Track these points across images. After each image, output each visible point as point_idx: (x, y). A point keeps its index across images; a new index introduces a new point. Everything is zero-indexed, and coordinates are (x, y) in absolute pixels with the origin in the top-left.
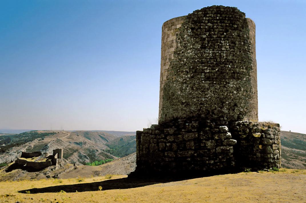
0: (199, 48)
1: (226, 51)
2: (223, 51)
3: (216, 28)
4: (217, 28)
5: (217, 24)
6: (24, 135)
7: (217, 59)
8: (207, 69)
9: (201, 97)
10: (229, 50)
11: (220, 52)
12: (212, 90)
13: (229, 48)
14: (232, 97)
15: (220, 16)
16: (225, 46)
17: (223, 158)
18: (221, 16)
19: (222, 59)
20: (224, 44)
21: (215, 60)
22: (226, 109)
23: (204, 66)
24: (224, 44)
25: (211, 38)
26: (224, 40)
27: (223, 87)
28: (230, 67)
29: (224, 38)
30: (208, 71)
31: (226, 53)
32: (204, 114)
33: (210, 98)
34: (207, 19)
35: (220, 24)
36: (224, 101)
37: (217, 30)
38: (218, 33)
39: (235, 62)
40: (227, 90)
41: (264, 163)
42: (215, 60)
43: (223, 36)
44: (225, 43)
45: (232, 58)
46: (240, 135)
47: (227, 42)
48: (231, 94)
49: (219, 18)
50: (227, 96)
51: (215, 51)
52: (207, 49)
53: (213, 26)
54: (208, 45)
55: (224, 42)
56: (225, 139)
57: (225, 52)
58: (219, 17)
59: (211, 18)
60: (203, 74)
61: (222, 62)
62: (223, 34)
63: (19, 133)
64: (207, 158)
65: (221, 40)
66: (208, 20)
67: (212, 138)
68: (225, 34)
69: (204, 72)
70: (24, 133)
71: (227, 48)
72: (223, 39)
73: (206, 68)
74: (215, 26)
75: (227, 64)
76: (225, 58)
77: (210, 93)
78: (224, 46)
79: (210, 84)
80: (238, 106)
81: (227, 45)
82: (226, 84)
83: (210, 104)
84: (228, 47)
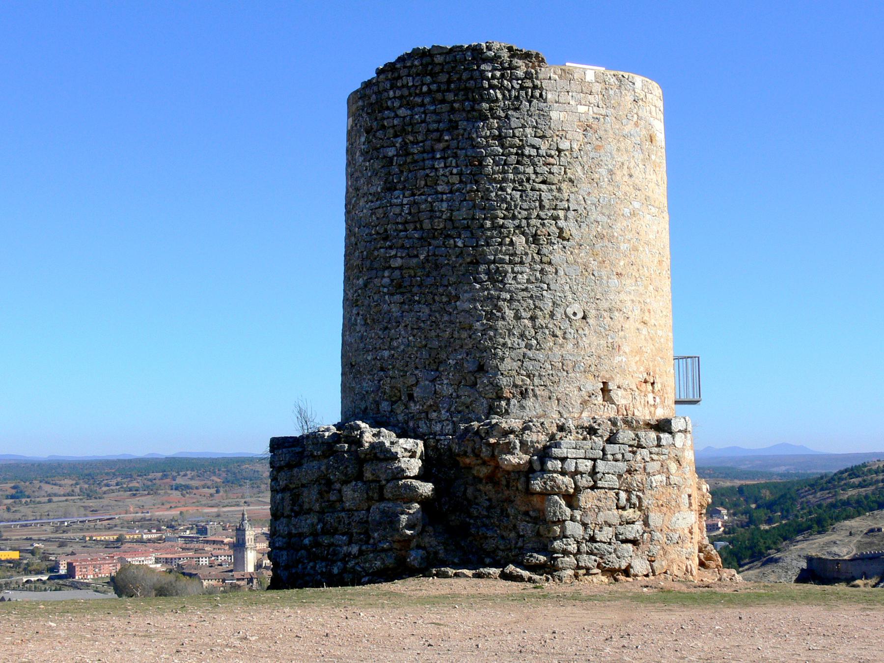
0: (379, 190)
1: (451, 192)
2: (440, 196)
3: (418, 123)
4: (423, 122)
5: (422, 109)
6: (856, 481)
7: (421, 222)
8: (395, 256)
9: (382, 347)
10: (458, 190)
11: (429, 199)
12: (408, 322)
13: (461, 182)
14: (466, 344)
15: (434, 82)
16: (447, 177)
17: (384, 539)
18: (434, 79)
19: (436, 220)
20: (441, 172)
21: (418, 226)
22: (445, 382)
23: (391, 248)
24: (441, 172)
25: (408, 154)
26: (444, 158)
27: (439, 312)
28: (460, 244)
29: (444, 150)
30: (398, 262)
31: (448, 201)
32: (386, 400)
33: (402, 347)
34: (398, 93)
35: (432, 108)
36: (443, 356)
37: (423, 128)
38: (426, 135)
39: (482, 226)
40: (451, 322)
41: (545, 562)
42: (418, 226)
43: (441, 145)
44: (446, 167)
45: (468, 214)
46: (469, 468)
47: (454, 164)
48: (464, 335)
49: (429, 87)
50: (452, 340)
51: (416, 197)
52: (396, 193)
53: (412, 116)
54: (401, 180)
55: (442, 165)
56: (388, 481)
57: (445, 196)
58: (428, 85)
59: (406, 92)
60: (386, 274)
61: (436, 230)
62: (439, 140)
63: (835, 471)
64: (343, 536)
65: (434, 158)
66: (401, 97)
67: (359, 477)
68: (446, 138)
69: (390, 267)
70: (853, 472)
71: (454, 184)
72: (438, 156)
73: (393, 253)
74: (417, 117)
75: (449, 236)
76: (444, 217)
77: (403, 332)
78: (445, 179)
79: (403, 303)
80: (487, 372)
81: (451, 174)
82: (449, 302)
83: (401, 368)
84: (455, 179)
